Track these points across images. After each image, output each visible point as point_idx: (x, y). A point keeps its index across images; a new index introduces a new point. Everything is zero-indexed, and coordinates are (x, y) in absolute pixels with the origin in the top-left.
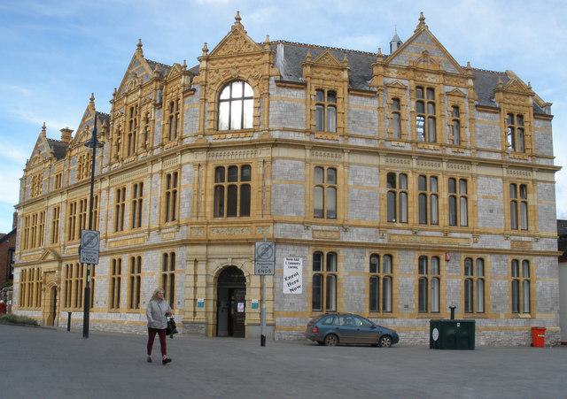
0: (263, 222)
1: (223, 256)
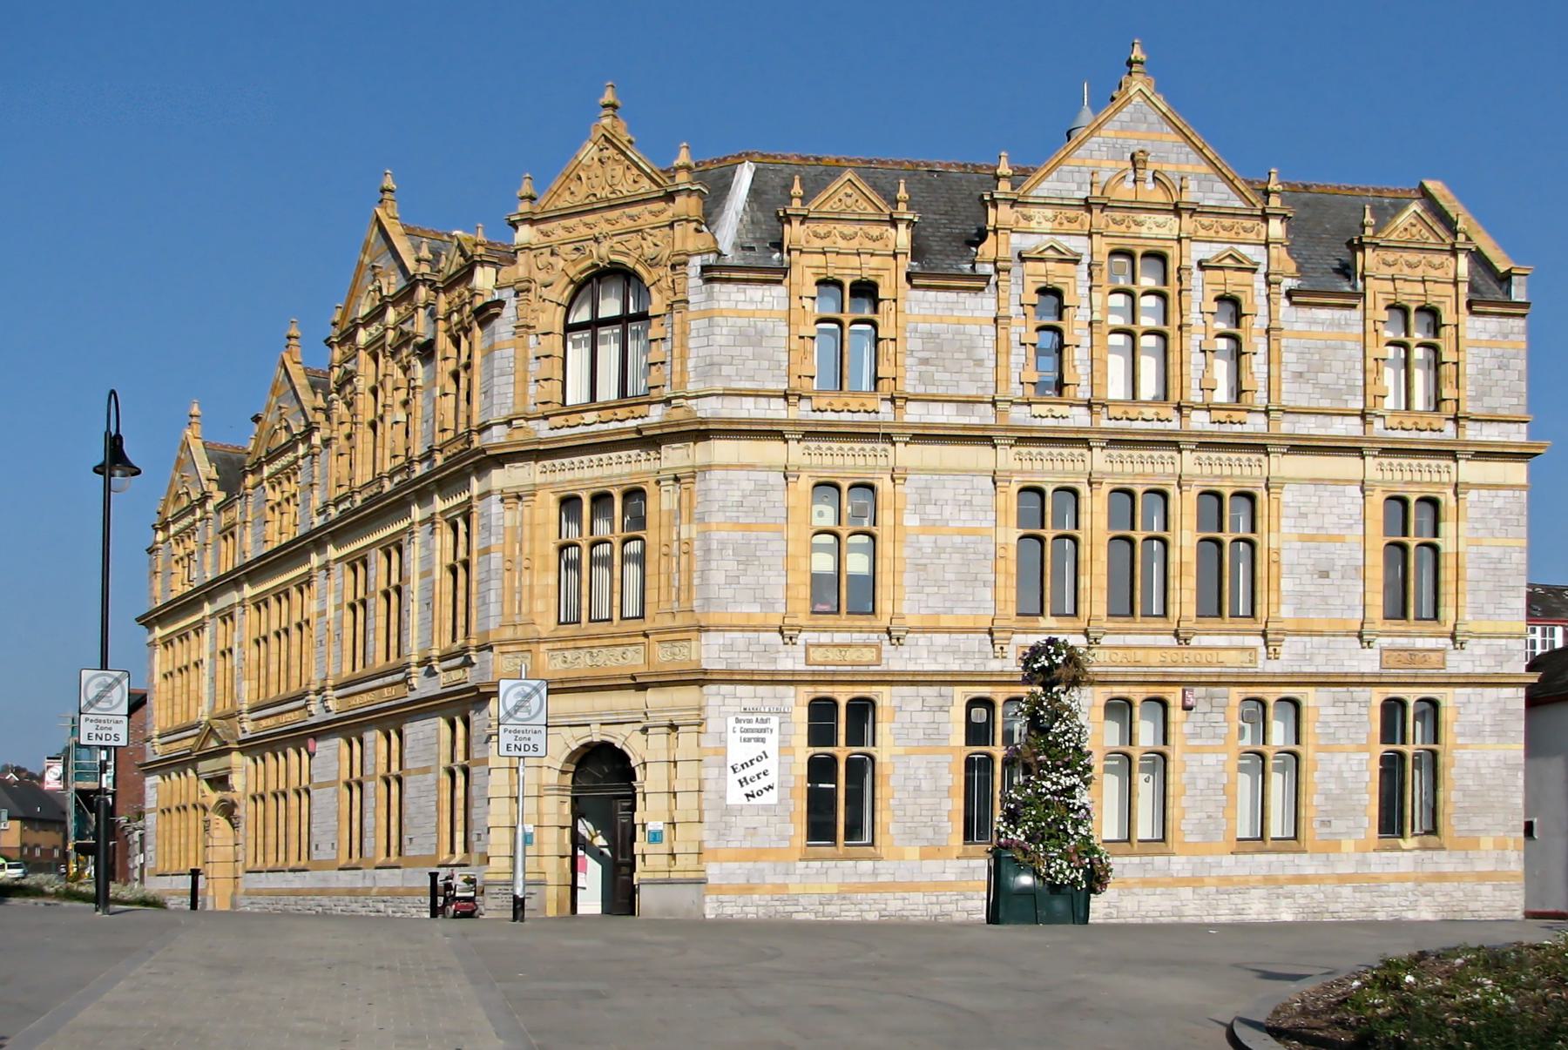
0: (671, 630)
1: (582, 720)
